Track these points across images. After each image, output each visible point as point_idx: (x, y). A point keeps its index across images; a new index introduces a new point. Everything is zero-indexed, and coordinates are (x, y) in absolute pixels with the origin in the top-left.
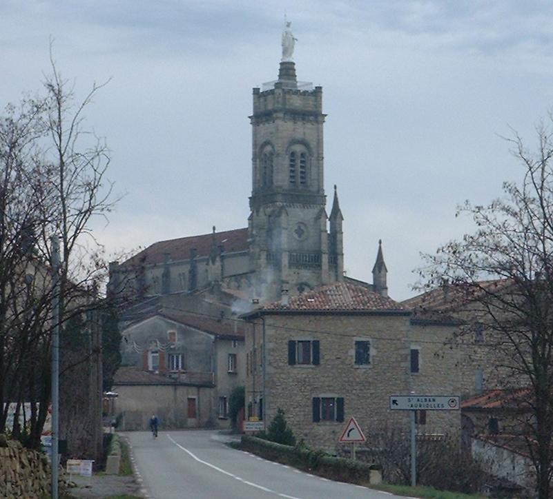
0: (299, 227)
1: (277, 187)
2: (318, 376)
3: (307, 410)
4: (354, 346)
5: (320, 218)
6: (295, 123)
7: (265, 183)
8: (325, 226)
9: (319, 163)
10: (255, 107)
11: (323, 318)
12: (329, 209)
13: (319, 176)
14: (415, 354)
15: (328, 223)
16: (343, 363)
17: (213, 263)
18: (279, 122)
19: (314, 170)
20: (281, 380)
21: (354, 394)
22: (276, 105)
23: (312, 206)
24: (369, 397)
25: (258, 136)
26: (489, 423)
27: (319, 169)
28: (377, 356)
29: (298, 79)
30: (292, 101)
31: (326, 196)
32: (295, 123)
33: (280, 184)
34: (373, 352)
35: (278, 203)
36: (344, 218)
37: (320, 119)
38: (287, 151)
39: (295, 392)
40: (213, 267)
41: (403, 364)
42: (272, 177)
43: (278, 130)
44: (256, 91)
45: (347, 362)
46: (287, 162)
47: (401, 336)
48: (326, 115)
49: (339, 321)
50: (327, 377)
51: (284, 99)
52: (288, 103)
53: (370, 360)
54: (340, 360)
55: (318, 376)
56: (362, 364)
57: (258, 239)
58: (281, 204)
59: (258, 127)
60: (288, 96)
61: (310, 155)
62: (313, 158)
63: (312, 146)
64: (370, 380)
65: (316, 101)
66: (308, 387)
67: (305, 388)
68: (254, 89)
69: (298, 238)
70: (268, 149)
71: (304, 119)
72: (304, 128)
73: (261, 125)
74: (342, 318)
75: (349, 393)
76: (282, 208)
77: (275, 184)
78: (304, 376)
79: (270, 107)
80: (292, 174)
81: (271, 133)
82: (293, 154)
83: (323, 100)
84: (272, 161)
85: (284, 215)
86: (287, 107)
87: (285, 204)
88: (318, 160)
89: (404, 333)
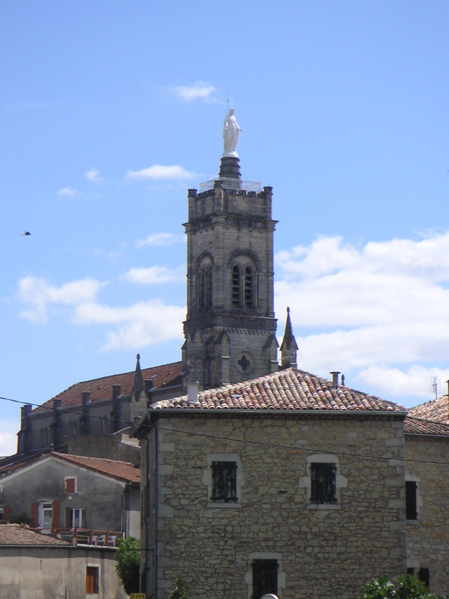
0: (244, 357)
1: (217, 307)
2: (247, 523)
3: (229, 582)
4: (309, 472)
5: (269, 346)
6: (239, 230)
7: (203, 304)
8: (276, 356)
9: (268, 280)
10: (191, 213)
11: (256, 424)
12: (280, 338)
13: (268, 295)
14: (411, 487)
15: (279, 354)
16: (290, 499)
17: (137, 399)
18: (219, 228)
19: (262, 288)
20: (185, 528)
21: (309, 554)
22: (216, 208)
23: (259, 331)
24: (334, 560)
25: (194, 247)
26: (375, 596)
27: (268, 287)
28: (348, 489)
29: (242, 178)
30: (235, 204)
31: (277, 320)
32: (239, 230)
33: (220, 304)
34: (341, 482)
35: (218, 328)
36: (299, 347)
37: (269, 226)
38: (229, 263)
39: (209, 550)
40: (137, 404)
41: (393, 504)
42: (211, 296)
43: (218, 238)
44: (192, 193)
45: (297, 499)
46: (229, 277)
47: (389, 455)
48: (277, 222)
49: (283, 430)
50: (263, 524)
51: (226, 201)
52: (230, 206)
53: (337, 495)
54: (285, 495)
55: (247, 523)
56: (322, 503)
57: (192, 370)
58: (222, 328)
59: (194, 237)
60: (230, 198)
61: (257, 270)
62: (260, 274)
63: (260, 259)
64: (337, 529)
65: (265, 204)
66: (230, 542)
67: (226, 542)
68: (189, 190)
69: (242, 371)
70: (207, 261)
71: (250, 225)
72: (251, 237)
73: (198, 234)
74: (289, 423)
75: (300, 552)
76: (223, 333)
77: (215, 304)
78: (224, 522)
79: (209, 211)
80: (235, 293)
81: (211, 243)
82: (236, 269)
83: (273, 203)
84: (211, 277)
85: (224, 341)
86: (230, 210)
87: (226, 328)
88: (268, 276)
89: (395, 450)
